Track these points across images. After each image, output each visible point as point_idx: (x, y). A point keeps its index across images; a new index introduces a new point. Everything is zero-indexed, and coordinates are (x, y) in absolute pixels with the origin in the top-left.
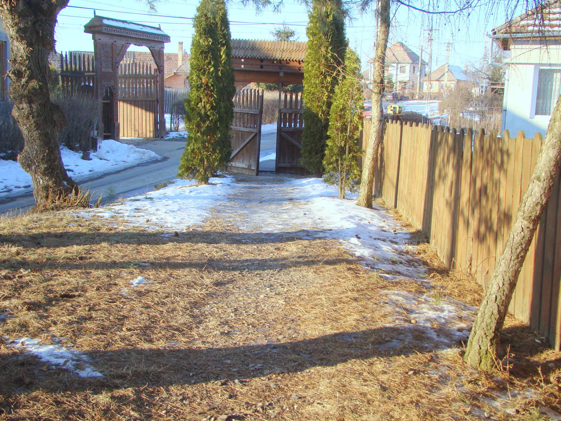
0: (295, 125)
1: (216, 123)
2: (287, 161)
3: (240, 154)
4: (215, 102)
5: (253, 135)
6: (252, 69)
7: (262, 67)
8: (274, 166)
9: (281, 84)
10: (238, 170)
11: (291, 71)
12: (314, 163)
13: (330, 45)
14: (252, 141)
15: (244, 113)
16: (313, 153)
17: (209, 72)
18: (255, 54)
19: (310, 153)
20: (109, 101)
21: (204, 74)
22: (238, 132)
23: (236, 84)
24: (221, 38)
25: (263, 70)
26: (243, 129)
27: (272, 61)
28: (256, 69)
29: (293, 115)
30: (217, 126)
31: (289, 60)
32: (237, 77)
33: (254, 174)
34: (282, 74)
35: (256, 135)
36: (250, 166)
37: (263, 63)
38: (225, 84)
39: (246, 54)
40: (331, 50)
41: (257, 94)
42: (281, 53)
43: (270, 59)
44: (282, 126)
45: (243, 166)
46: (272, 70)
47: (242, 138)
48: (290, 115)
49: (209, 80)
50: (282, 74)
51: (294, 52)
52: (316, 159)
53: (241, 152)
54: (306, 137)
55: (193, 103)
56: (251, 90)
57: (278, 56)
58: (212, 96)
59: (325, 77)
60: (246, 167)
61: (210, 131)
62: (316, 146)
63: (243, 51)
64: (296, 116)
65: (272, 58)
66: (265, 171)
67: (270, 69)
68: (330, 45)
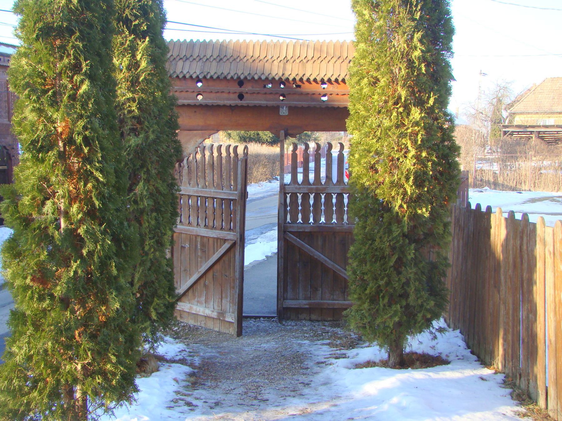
0: (316, 219)
1: (103, 265)
2: (301, 295)
3: (199, 287)
4: (101, 196)
5: (227, 246)
6: (221, 103)
7: (241, 97)
8: (275, 308)
9: (282, 133)
10: (196, 320)
11: (305, 104)
12: (386, 327)
13: (417, 28)
14: (226, 258)
15: (206, 198)
16: (383, 302)
17: (73, 98)
18: (227, 70)
19: (374, 300)
20: (5, 167)
21: (54, 103)
22: (193, 238)
23: (182, 136)
24: (136, 17)
25: (244, 103)
26: (204, 232)
27: (263, 81)
28: (228, 103)
29: (312, 196)
30: (109, 273)
31: (301, 80)
32: (184, 119)
33: (233, 330)
34: (284, 112)
35: (234, 245)
36: (222, 314)
37: (244, 89)
38: (152, 137)
39: (206, 70)
40: (420, 41)
41: (232, 155)
42: (282, 65)
43: (260, 78)
44: (288, 219)
45: (208, 312)
46: (263, 103)
47: (203, 251)
48: (306, 197)
49: (75, 122)
50: (284, 112)
51: (310, 63)
52: (391, 317)
53: (202, 281)
54: (363, 262)
55: (26, 200)
56: (220, 147)
57: (276, 71)
58: (87, 176)
59: (407, 108)
60: (215, 315)
61: (91, 286)
62: (388, 284)
63: (200, 64)
64: (317, 198)
65: (263, 77)
66: (256, 318)
67: (261, 101)
68: (417, 28)
